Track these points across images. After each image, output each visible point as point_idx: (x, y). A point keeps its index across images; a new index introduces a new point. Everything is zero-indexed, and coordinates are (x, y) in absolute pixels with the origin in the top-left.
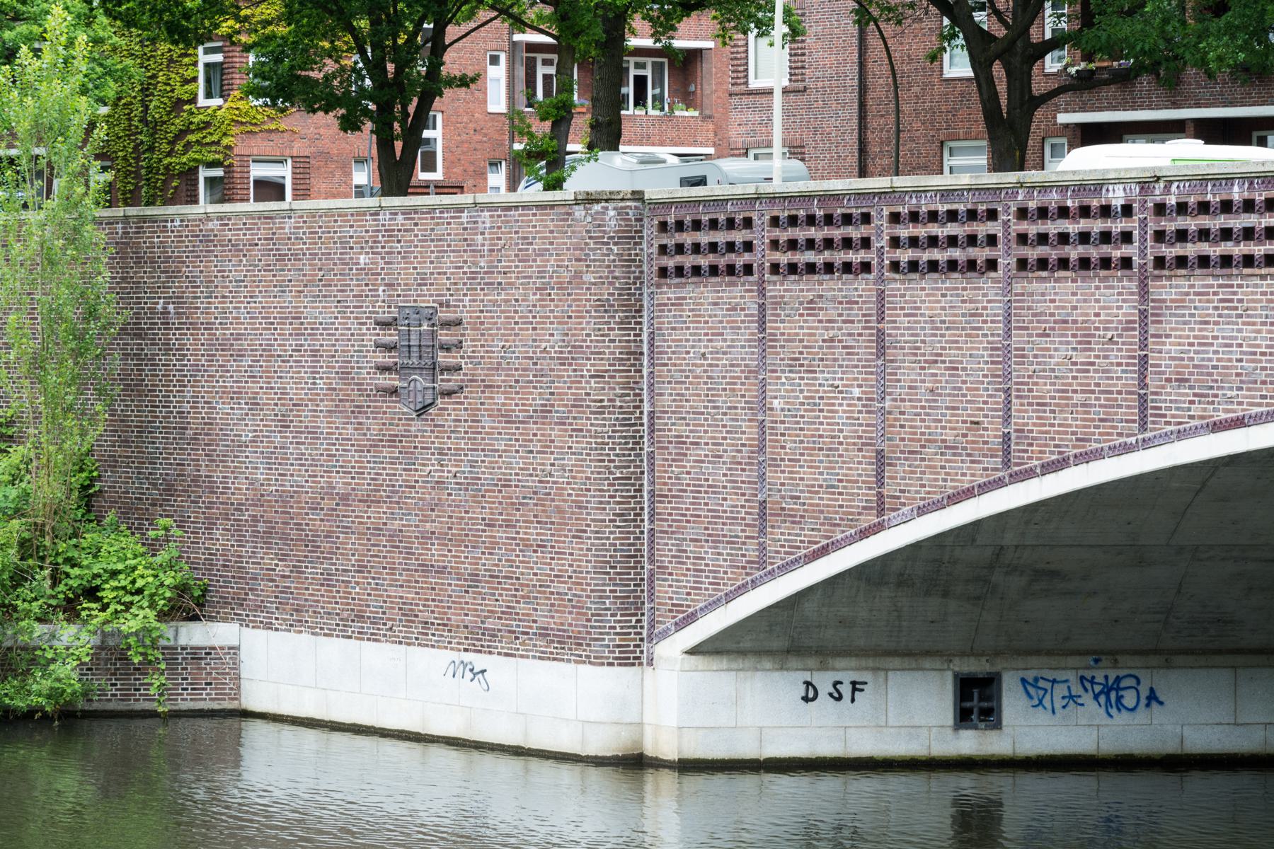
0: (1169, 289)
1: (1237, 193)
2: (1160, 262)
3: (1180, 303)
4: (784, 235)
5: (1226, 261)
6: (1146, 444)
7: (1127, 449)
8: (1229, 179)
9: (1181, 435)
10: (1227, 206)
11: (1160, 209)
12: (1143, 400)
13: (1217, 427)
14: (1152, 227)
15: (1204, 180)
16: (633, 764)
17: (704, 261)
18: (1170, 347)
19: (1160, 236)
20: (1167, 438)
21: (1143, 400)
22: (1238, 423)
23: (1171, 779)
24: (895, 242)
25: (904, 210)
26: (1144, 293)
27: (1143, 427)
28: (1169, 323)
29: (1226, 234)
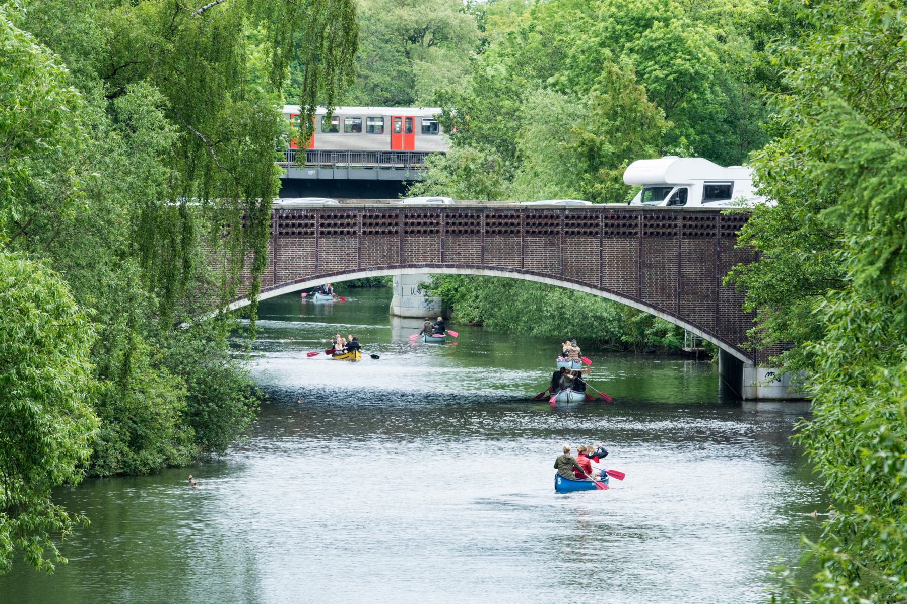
0: (282, 242)
1: (509, 213)
2: (684, 234)
3: (286, 245)
4: (610, 222)
5: (300, 233)
6: (276, 288)
7: (271, 289)
8: (301, 210)
9: (287, 285)
10: (300, 217)
11: (281, 217)
12: (275, 274)
13: (297, 282)
14: (565, 222)
15: (575, 210)
16: (385, 413)
17: (422, 229)
18: (283, 259)
19: (567, 225)
20: (283, 286)
21: (275, 274)
22: (303, 281)
23: (793, 404)
24: (364, 225)
25: (503, 214)
26: (276, 243)
27: (275, 283)
28: (283, 251)
29: (300, 225)
